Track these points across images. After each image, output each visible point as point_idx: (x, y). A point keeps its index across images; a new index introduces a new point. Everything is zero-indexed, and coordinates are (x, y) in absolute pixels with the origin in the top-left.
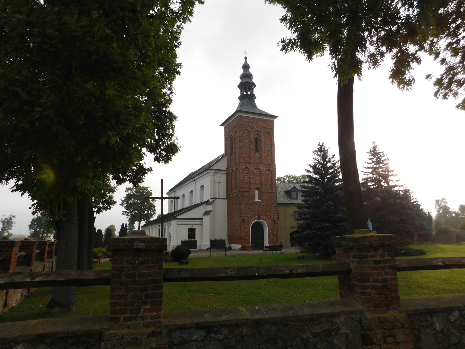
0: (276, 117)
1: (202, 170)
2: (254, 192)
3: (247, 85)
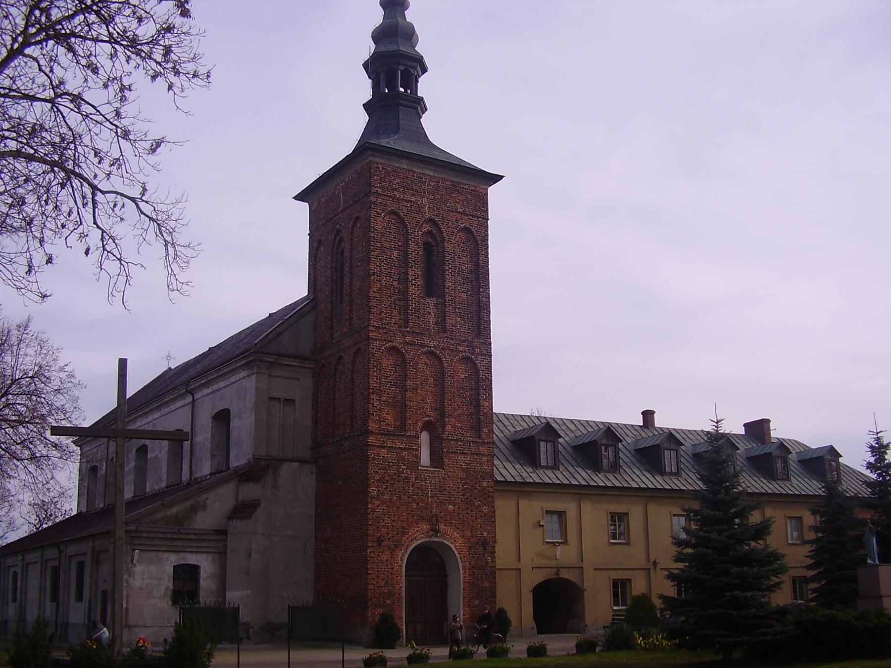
0: (496, 178)
1: (206, 362)
2: (417, 437)
3: (395, 67)
